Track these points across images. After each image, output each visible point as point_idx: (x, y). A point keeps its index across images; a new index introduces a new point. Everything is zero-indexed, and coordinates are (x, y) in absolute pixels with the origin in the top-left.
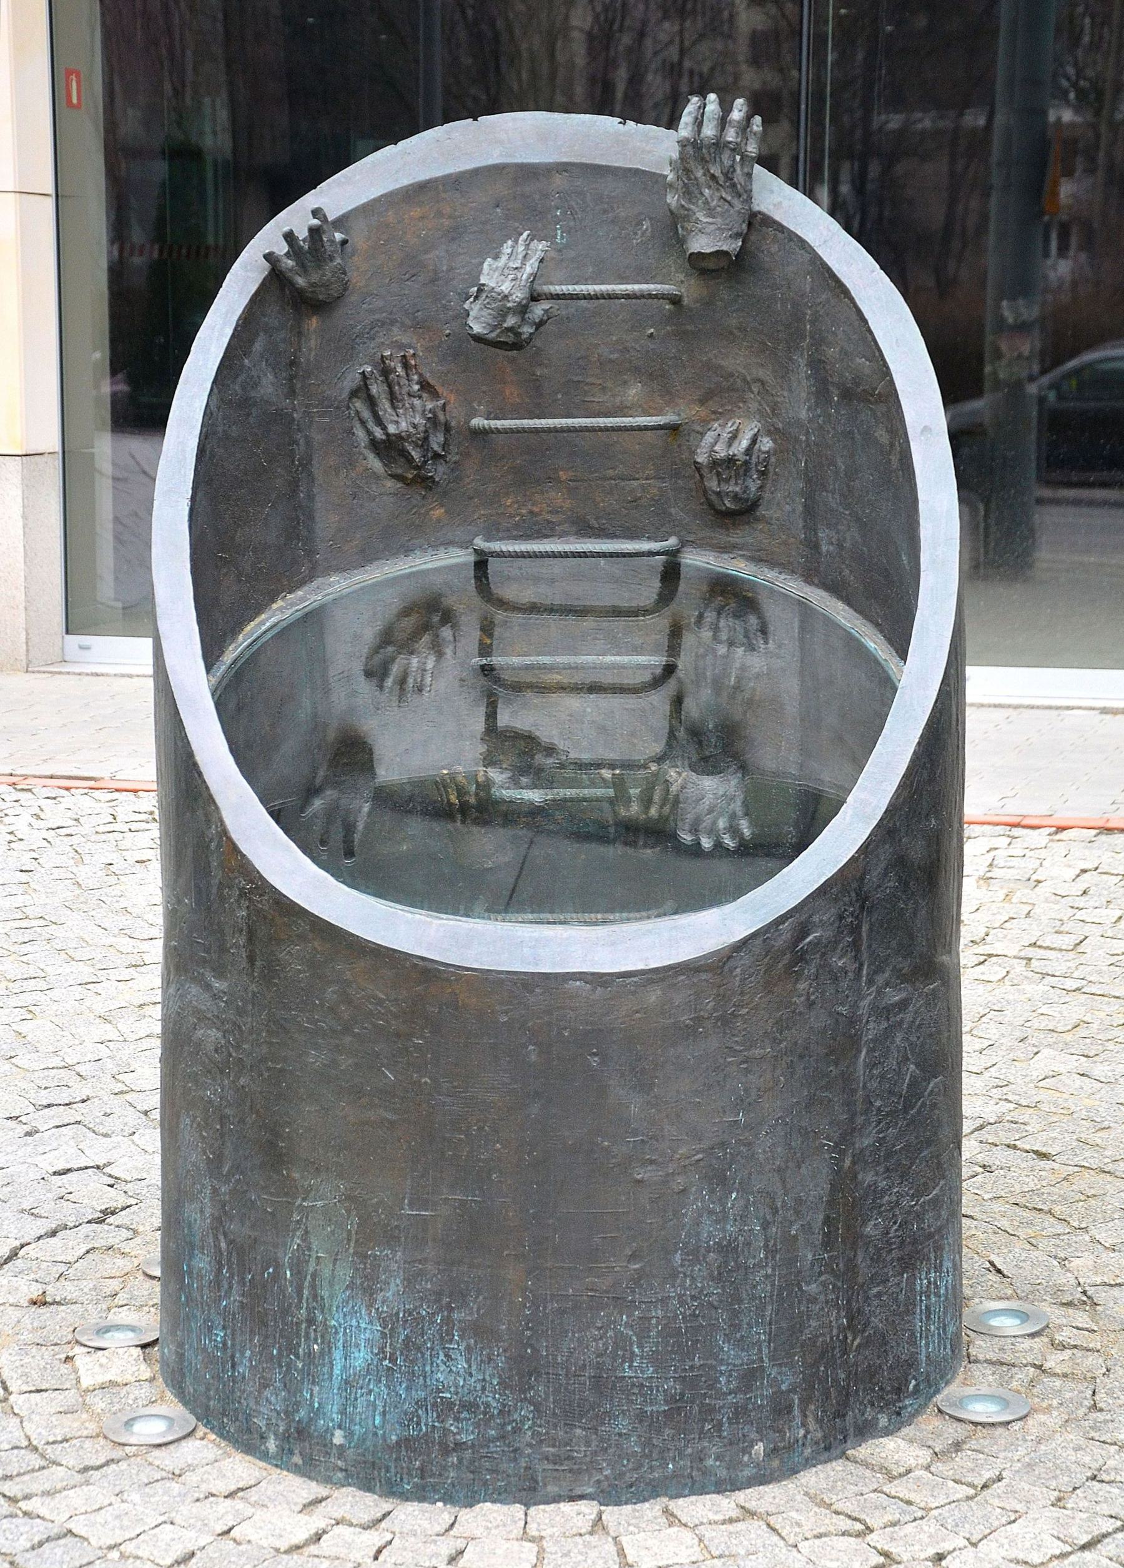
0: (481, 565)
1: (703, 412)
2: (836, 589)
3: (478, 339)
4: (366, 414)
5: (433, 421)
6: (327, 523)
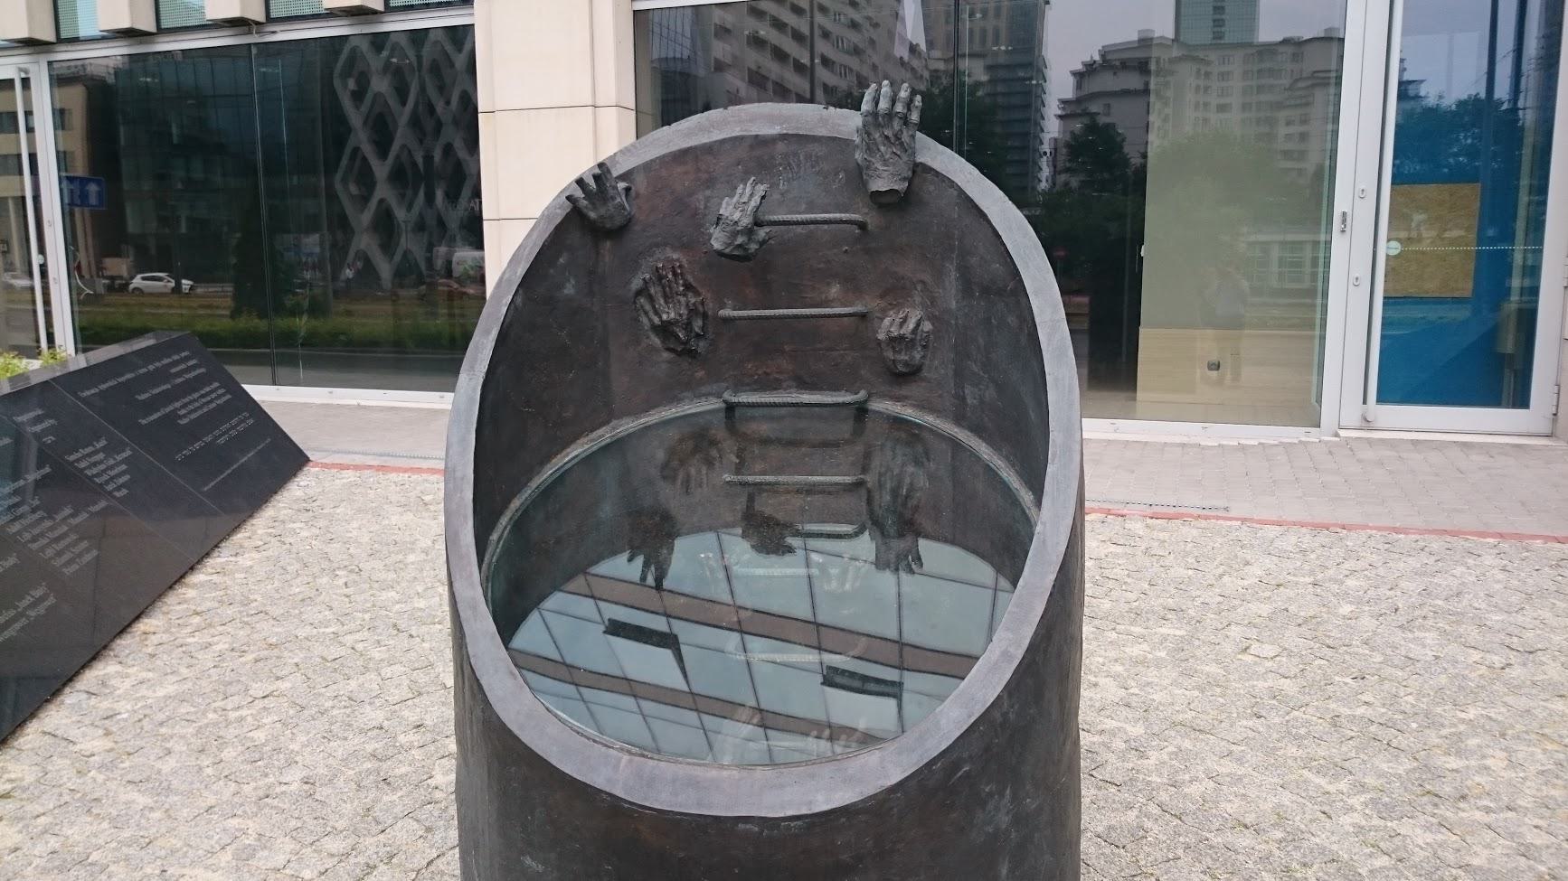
0: (730, 408)
1: (883, 304)
2: (978, 430)
3: (720, 254)
4: (648, 307)
5: (693, 311)
6: (620, 382)
